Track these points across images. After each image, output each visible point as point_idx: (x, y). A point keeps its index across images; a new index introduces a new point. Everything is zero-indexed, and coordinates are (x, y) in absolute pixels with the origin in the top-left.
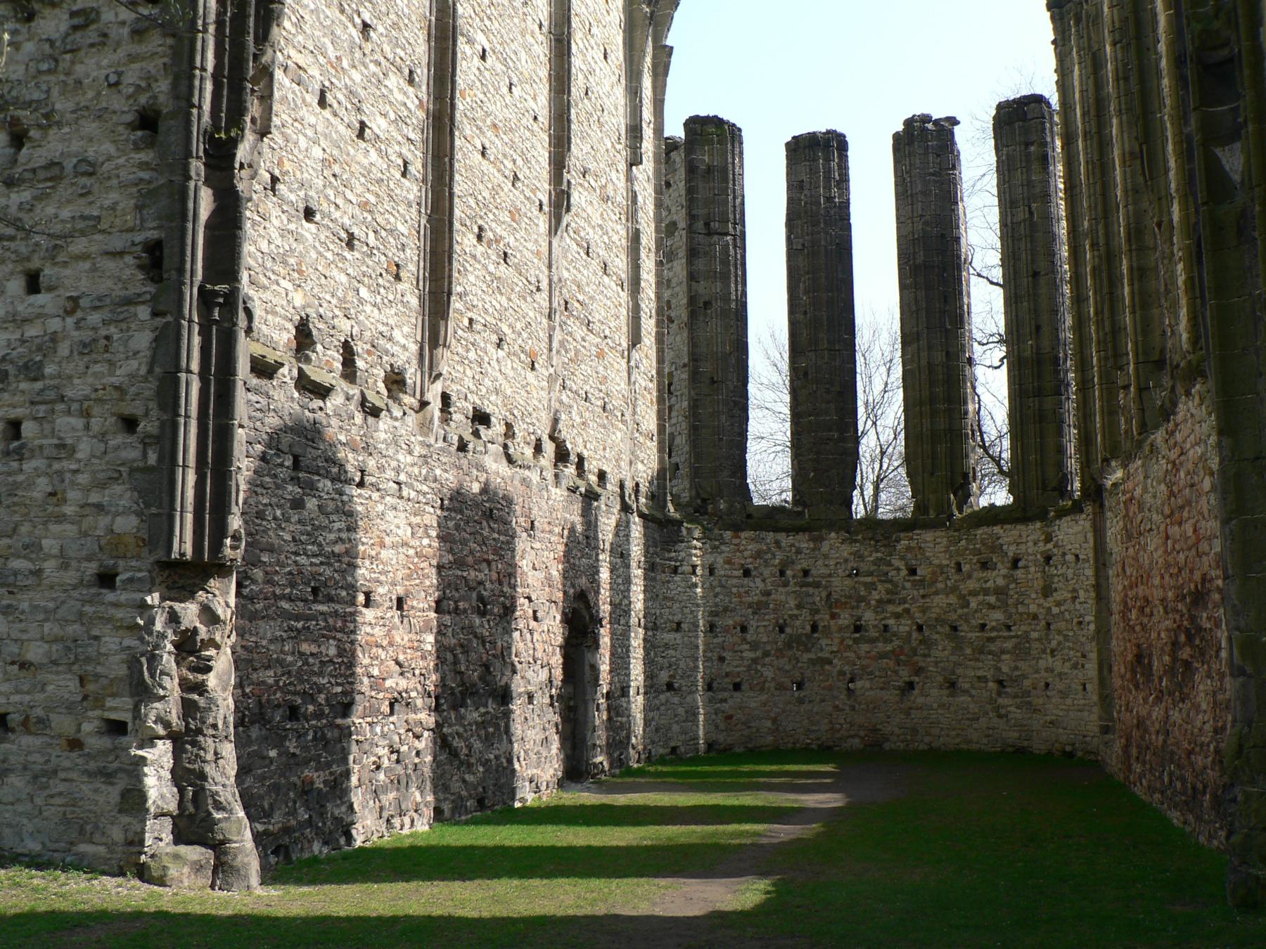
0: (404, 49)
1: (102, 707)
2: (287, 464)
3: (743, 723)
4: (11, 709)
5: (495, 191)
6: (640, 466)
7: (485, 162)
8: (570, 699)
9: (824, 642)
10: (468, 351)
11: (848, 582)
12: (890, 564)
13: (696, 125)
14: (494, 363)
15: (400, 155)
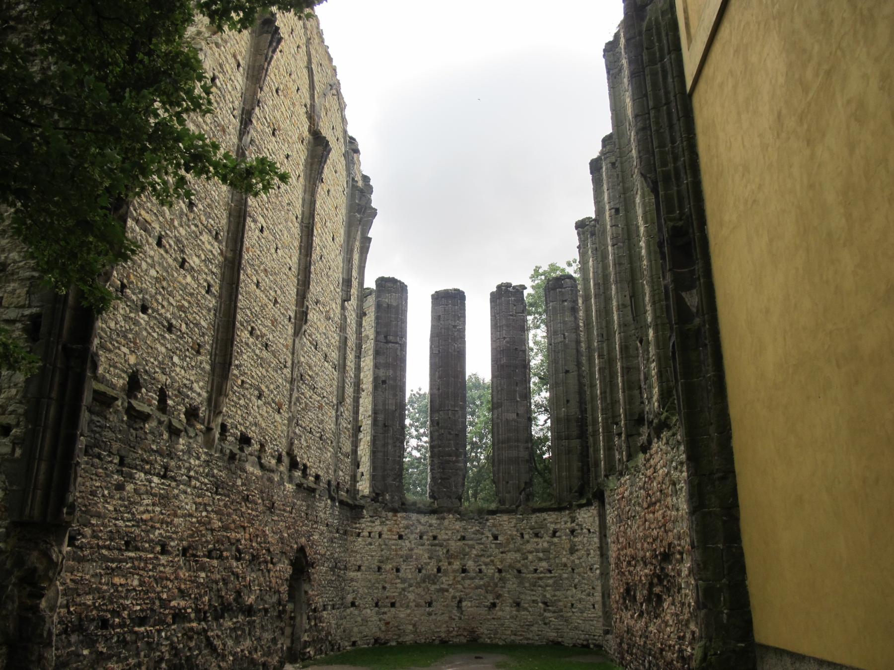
0: (214, 220)
3: (397, 627)
5: (263, 307)
6: (341, 473)
7: (258, 291)
9: (444, 579)
10: (240, 399)
11: (459, 543)
12: (483, 534)
13: (383, 282)
15: (206, 280)
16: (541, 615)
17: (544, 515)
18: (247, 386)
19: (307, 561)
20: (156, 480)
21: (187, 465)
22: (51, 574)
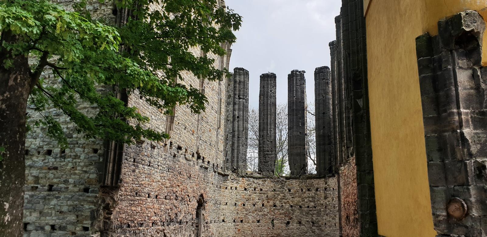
1: (83, 223)
2: (132, 161)
4: (56, 224)
6: (218, 160)
8: (197, 224)
9: (265, 210)
10: (177, 131)
11: (273, 193)
12: (283, 188)
14: (184, 134)
16: (311, 228)
17: (313, 180)
18: (180, 125)
19: (204, 201)
20: (146, 167)
21: (158, 160)
22: (114, 206)
